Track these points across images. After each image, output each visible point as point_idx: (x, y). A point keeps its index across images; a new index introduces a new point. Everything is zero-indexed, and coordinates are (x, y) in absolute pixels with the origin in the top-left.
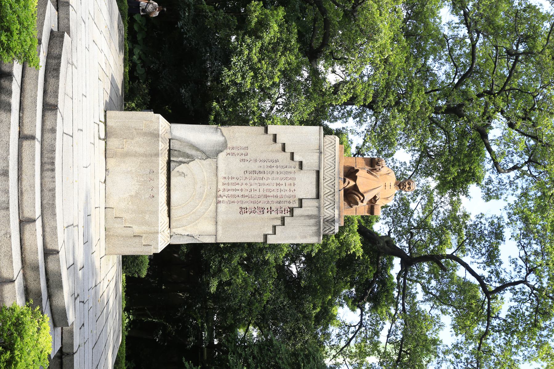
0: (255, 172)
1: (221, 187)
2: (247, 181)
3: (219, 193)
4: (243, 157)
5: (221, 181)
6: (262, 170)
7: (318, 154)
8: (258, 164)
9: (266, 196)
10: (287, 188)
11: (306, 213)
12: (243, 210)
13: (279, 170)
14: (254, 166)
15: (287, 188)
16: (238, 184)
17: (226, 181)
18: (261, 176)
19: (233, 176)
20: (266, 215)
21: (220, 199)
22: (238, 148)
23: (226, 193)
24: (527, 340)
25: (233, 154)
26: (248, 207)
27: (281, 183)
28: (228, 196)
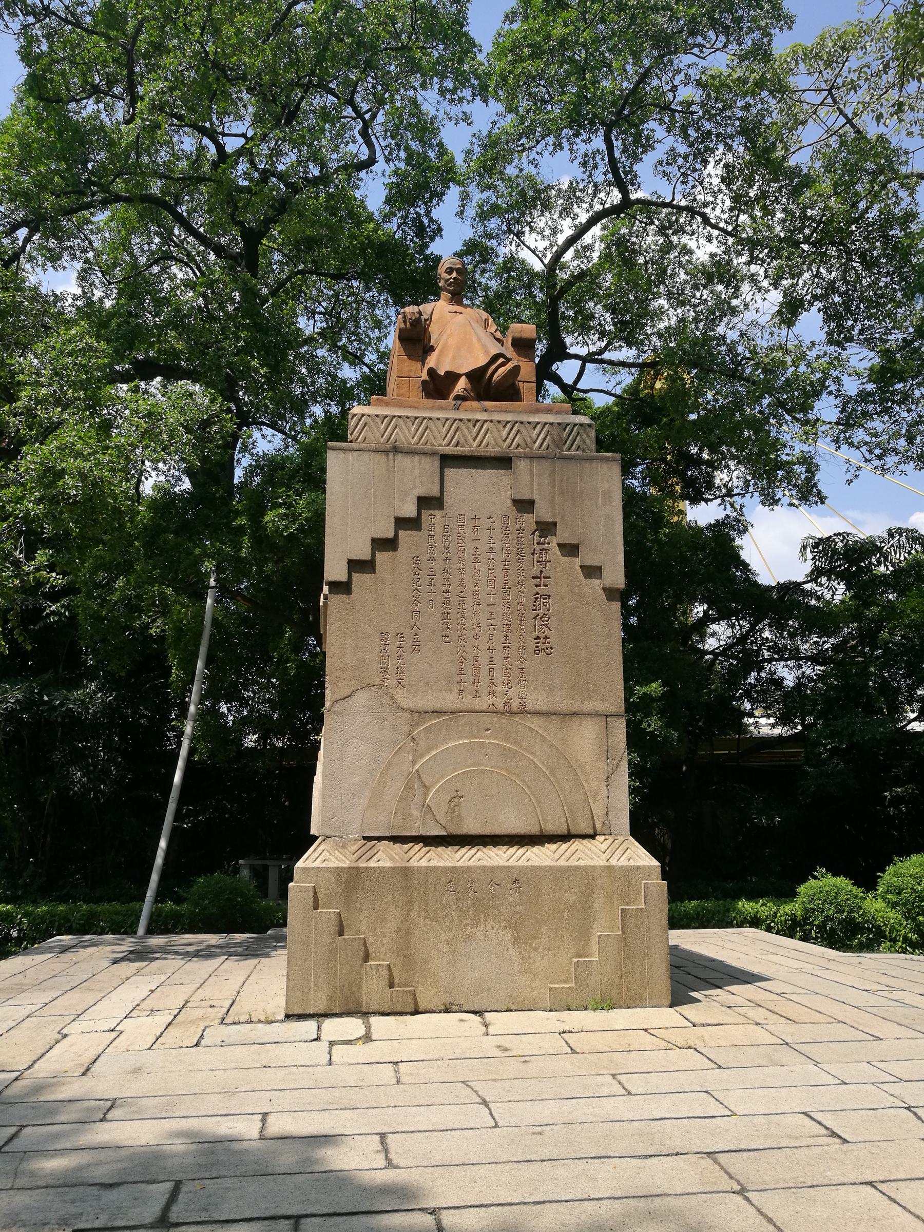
1: (483, 702)
4: (407, 644)
5: (467, 701)
7: (399, 457)
12: (542, 645)
14: (431, 618)
19: (455, 670)
22: (384, 655)
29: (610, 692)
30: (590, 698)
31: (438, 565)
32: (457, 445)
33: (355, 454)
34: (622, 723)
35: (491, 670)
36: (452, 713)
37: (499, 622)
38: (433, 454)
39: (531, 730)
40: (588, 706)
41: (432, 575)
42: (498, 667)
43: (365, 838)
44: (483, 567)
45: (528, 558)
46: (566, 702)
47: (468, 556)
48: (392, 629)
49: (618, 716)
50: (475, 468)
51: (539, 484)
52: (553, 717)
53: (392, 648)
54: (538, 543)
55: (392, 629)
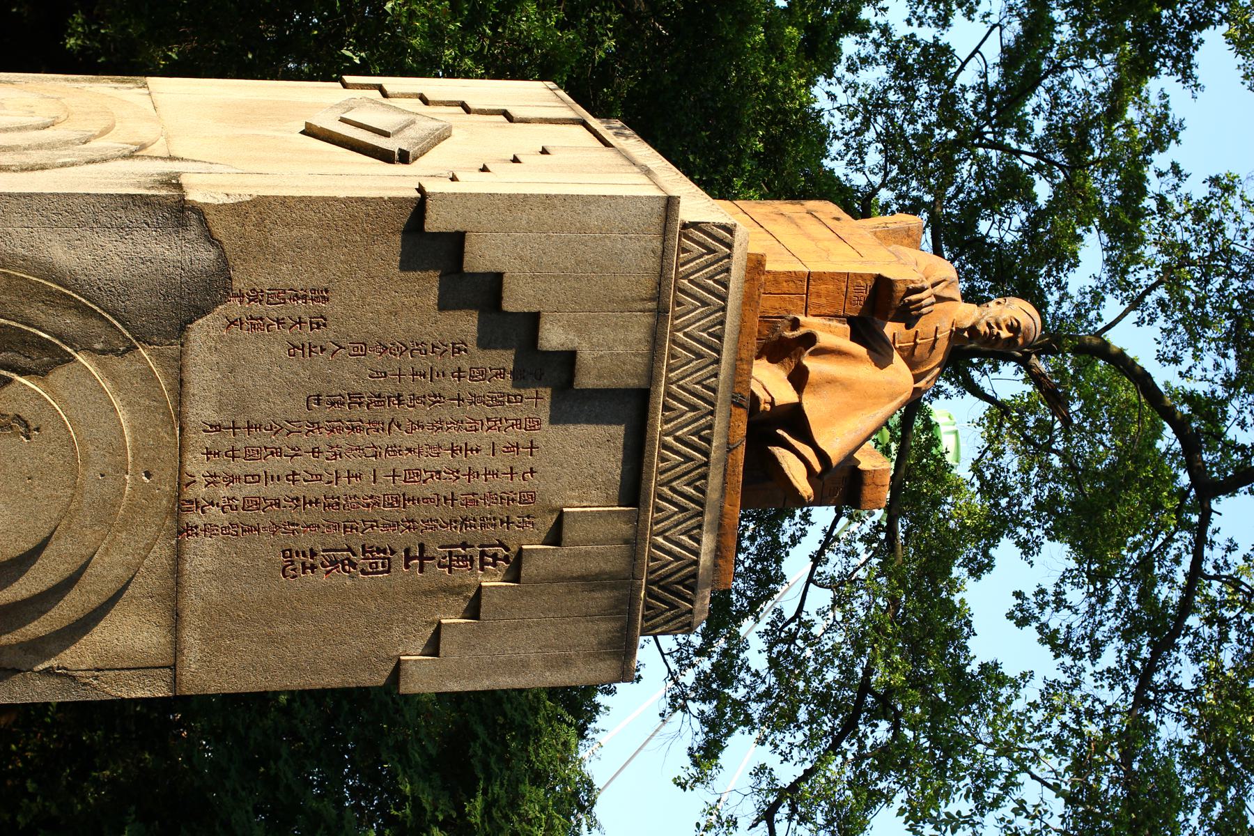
0: (355, 399)
1: (197, 465)
3: (190, 493)
4: (306, 335)
5: (199, 439)
6: (389, 389)
7: (647, 319)
8: (375, 359)
10: (499, 463)
11: (577, 568)
12: (296, 562)
14: (349, 374)
15: (499, 463)
16: (277, 452)
17: (225, 441)
18: (385, 414)
19: (257, 417)
21: (194, 518)
22: (279, 295)
23: (223, 492)
25: (257, 322)
28: (229, 505)
29: (204, 673)
30: (206, 640)
31: (449, 385)
32: (666, 408)
33: (657, 244)
34: (161, 691)
35: (256, 478)
36: (180, 415)
37: (343, 488)
39: (149, 548)
40: (191, 637)
41: (432, 374)
42: (257, 467)
45: (458, 534)
46: (200, 604)
48: (331, 308)
49: (175, 682)
50: (625, 446)
52: (171, 582)
54: (483, 554)
55: (331, 308)
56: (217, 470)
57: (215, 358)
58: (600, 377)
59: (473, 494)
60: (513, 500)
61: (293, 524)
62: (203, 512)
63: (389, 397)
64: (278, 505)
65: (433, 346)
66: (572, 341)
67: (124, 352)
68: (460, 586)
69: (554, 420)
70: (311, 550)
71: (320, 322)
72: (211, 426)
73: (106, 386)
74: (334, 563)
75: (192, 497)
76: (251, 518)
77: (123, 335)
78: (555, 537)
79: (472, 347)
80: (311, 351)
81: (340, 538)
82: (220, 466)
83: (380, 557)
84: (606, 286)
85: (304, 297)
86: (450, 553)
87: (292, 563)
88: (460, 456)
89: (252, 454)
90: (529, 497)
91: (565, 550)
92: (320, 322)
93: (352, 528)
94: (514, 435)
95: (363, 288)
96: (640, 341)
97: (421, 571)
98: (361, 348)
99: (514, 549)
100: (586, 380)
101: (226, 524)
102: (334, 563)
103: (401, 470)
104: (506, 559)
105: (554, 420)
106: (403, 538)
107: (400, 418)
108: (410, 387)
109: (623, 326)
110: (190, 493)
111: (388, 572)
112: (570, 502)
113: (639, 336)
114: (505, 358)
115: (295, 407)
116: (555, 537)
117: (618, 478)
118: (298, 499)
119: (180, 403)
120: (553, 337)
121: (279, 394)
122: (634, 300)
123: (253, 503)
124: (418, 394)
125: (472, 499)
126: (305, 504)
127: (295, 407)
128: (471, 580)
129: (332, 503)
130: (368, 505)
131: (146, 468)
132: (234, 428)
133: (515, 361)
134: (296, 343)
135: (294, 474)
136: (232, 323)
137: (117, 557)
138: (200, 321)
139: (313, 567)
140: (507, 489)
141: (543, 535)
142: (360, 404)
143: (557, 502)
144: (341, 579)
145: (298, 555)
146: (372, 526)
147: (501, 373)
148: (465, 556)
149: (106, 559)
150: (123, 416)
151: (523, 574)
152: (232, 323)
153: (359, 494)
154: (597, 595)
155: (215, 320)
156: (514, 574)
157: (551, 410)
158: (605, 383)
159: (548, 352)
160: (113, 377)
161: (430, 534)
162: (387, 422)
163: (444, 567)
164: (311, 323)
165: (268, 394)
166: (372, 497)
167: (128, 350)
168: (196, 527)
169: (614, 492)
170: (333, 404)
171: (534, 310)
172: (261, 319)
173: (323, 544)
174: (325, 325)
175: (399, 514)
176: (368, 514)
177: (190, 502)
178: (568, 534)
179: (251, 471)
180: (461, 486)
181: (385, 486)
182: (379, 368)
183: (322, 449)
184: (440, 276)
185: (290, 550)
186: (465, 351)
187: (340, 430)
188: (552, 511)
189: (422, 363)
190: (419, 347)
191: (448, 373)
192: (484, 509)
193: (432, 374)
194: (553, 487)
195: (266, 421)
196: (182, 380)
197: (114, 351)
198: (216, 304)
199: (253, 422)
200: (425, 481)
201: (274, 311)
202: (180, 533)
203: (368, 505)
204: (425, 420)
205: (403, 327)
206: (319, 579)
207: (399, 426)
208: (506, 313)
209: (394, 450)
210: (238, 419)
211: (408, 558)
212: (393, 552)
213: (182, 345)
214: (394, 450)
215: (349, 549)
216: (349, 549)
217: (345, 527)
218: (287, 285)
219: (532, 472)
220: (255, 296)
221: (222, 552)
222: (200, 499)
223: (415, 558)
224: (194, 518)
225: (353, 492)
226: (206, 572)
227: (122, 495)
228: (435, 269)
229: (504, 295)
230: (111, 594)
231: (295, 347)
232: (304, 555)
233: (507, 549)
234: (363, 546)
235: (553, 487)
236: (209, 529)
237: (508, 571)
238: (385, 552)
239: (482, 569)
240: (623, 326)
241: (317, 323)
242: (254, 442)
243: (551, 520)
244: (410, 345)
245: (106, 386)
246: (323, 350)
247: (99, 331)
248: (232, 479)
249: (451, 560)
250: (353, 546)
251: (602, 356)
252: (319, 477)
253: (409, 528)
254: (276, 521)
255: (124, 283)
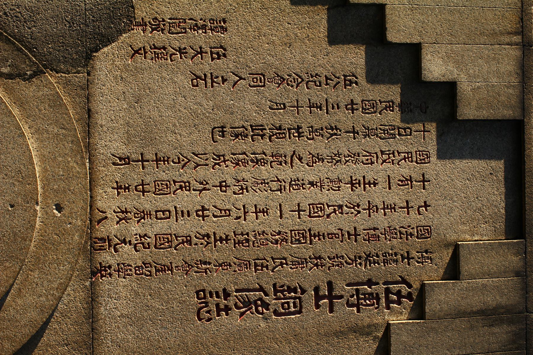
0: (258, 131)
1: (108, 201)
2: (228, 172)
3: (102, 230)
4: (207, 65)
5: (110, 173)
6: (288, 120)
7: (515, 52)
8: (272, 91)
9: (308, 236)
10: (397, 196)
11: (476, 302)
12: (210, 303)
13: (361, 119)
14: (250, 105)
15: (397, 196)
16: (185, 186)
17: (134, 175)
18: (287, 146)
19: (165, 150)
20: (313, 316)
21: (107, 257)
22: (179, 25)
23: (135, 228)
24: (10, 61)
25: (159, 52)
26: (232, 288)
27: (369, 177)
28: (140, 242)
36: (89, 147)
37: (251, 224)
38: (524, 107)
41: (328, 106)
42: (166, 202)
43: (280, 205)
44: (344, 195)
45: (363, 271)
47: (359, 170)
50: (506, 178)
51: (484, 286)
52: (86, 328)
53: (200, 39)
54: (388, 291)
56: (128, 205)
57: (121, 87)
58: (479, 108)
59: (375, 229)
60: (411, 235)
61: (205, 263)
62: (116, 251)
63: (289, 129)
64: (189, 242)
65: (327, 78)
66: (451, 72)
67: (32, 77)
68: (369, 326)
69: (441, 156)
70: (224, 290)
71: (219, 53)
72: (120, 159)
73: (16, 112)
74: (247, 304)
75: (104, 235)
76: (165, 256)
77: (29, 58)
78: (453, 272)
79: (362, 80)
80: (213, 82)
81: (250, 277)
82: (129, 201)
83: (291, 296)
84: (477, 21)
85: (204, 27)
86: (357, 291)
87: (207, 303)
88: (359, 190)
89: (162, 188)
90: (425, 232)
91: (464, 284)
92: (219, 53)
93: (262, 266)
94: (406, 169)
95: (258, 19)
96: (510, 74)
97: (331, 311)
98: (260, 79)
99: (416, 285)
100: (468, 111)
101: (140, 263)
102: (247, 304)
103: (305, 205)
104: (409, 296)
105: (441, 156)
106: (312, 277)
107: (301, 151)
108: (308, 119)
109: (494, 59)
110: (102, 230)
111: (300, 312)
112: (463, 236)
113: (509, 68)
114: (393, 93)
115: (200, 141)
116: (453, 272)
117: (503, 211)
118: (208, 236)
119: (89, 134)
120: (435, 68)
121: (185, 125)
122: (502, 34)
123: (165, 241)
124: (316, 127)
125: (373, 235)
126: (216, 241)
127: (200, 141)
128: (378, 320)
129: (242, 240)
130: (277, 242)
131: (56, 200)
132: (143, 161)
133: (402, 95)
134: (199, 73)
135: (203, 209)
136: (137, 52)
137: (30, 299)
138: (106, 49)
139: (227, 309)
140: (405, 224)
141: (441, 271)
142: (262, 136)
143: (452, 237)
144: (254, 321)
145: (211, 296)
146: (281, 264)
147: (390, 106)
148: (371, 294)
149: (20, 302)
150: (32, 144)
151: (427, 310)
152: (137, 52)
153: (267, 230)
154: (496, 330)
155: (119, 49)
156: (419, 312)
157: (438, 144)
158: (484, 114)
159: (431, 83)
160: (21, 104)
161: (337, 272)
162: (289, 154)
163: (352, 305)
164: (212, 53)
165: (174, 125)
166: (279, 233)
167: (35, 74)
168: (110, 267)
169: (501, 225)
170: (237, 136)
171: (415, 41)
172: (164, 48)
173: (236, 284)
174: (224, 55)
175: (305, 251)
176: (276, 251)
177: (103, 240)
178: (465, 267)
179: (161, 206)
180: (362, 222)
181: (291, 222)
182: (279, 100)
183: (229, 182)
184: (328, 9)
185: (204, 291)
186: (356, 83)
187: (245, 163)
188: (447, 245)
189: (318, 95)
190: (313, 79)
191: (342, 105)
192: (386, 245)
193: (328, 106)
194: (445, 221)
195: (173, 154)
196: (89, 110)
197: (22, 76)
198: (120, 33)
199: (160, 155)
200: (328, 216)
201: (175, 41)
202: (94, 274)
203: (277, 242)
204: (325, 152)
205: (297, 58)
206: (232, 321)
207: (300, 159)
208: (391, 43)
209: (297, 184)
210: (145, 152)
211: (318, 298)
212: (303, 291)
213: (89, 74)
214: (297, 184)
215: (261, 289)
216: (261, 289)
217: (256, 265)
218: (186, 14)
219: (426, 206)
220: (157, 26)
221: (137, 294)
222: (112, 237)
223: (324, 297)
224: (107, 257)
225: (261, 229)
226: (122, 316)
227: (33, 227)
228: (323, 5)
229: (387, 26)
230: (25, 340)
231: (198, 77)
232: (218, 296)
233: (410, 286)
234: (274, 285)
235: (445, 221)
236: (122, 269)
237: (412, 309)
238: (296, 292)
239: (388, 308)
240: (494, 59)
241: (218, 53)
242: (163, 176)
243: (447, 255)
244: (305, 76)
245: (16, 112)
246: (224, 80)
247: (5, 54)
248: (143, 215)
249: (358, 299)
250: (264, 286)
251: (479, 88)
252: (227, 213)
253: (316, 265)
254: (188, 259)
255: (29, 9)
